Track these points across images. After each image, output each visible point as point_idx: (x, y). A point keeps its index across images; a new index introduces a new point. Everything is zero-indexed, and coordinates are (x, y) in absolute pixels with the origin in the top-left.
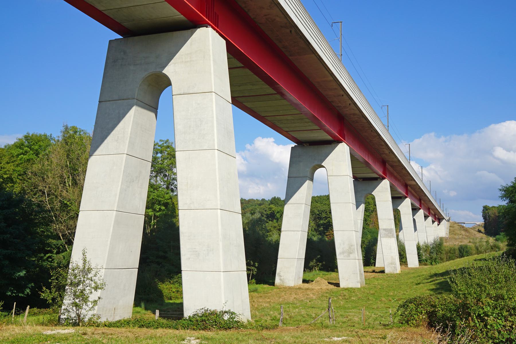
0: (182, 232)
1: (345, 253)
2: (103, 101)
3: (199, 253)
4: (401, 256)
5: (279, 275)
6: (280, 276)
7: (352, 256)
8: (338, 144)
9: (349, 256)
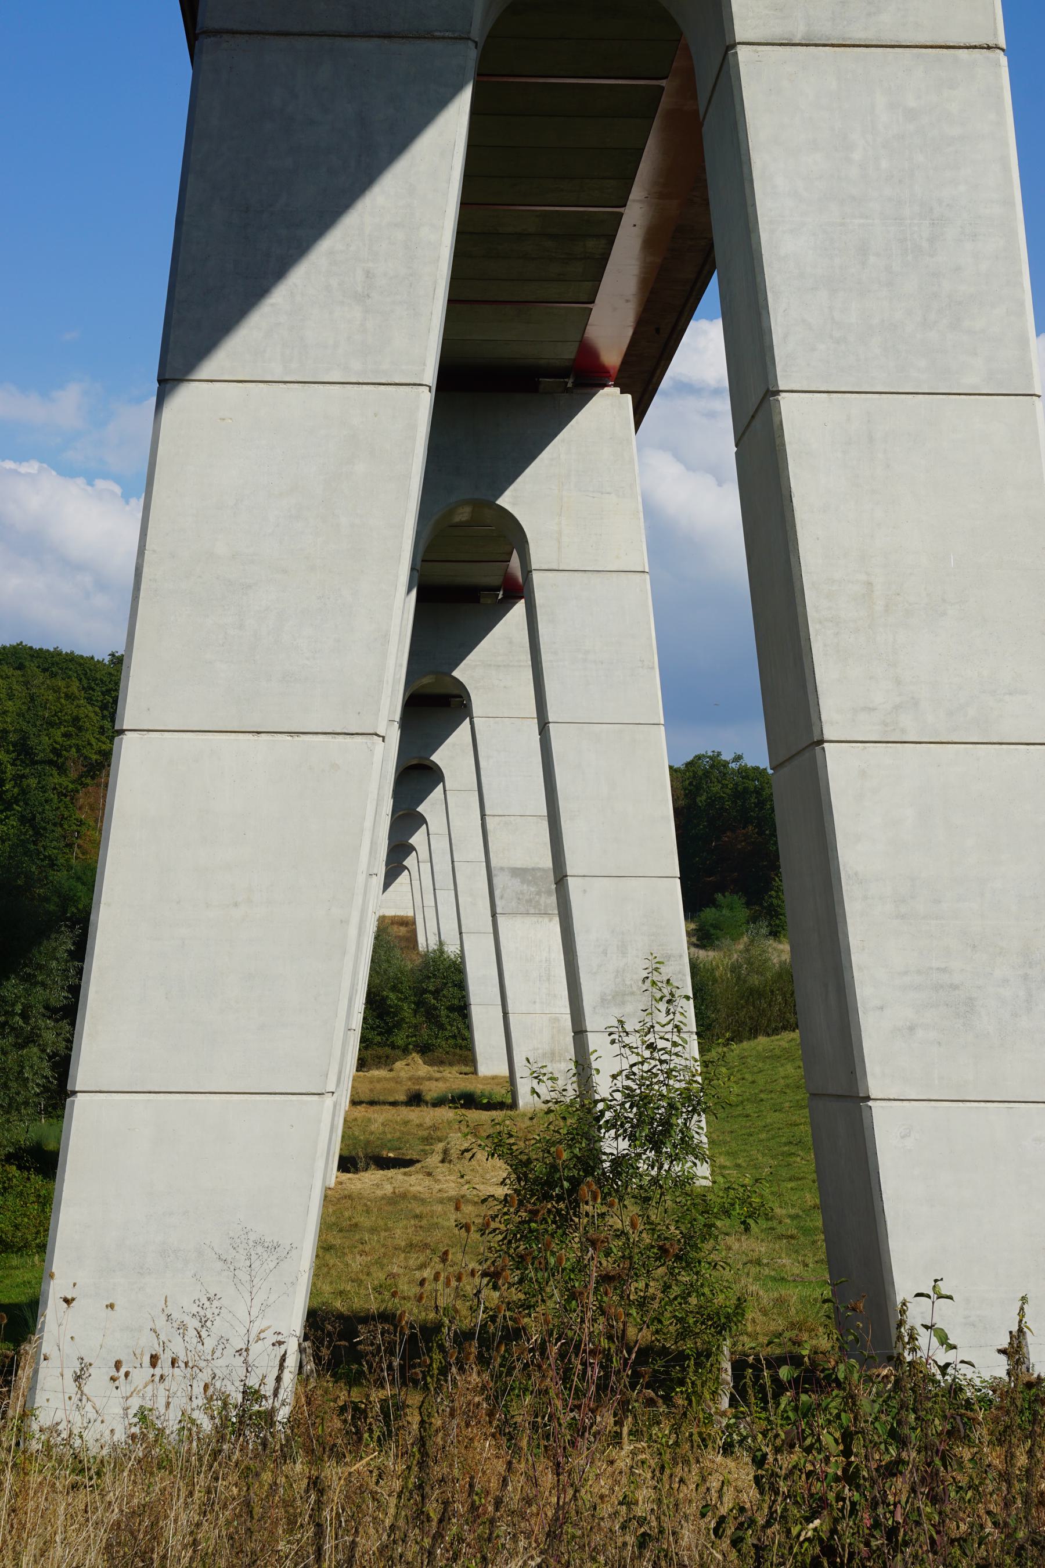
0: (856, 874)
1: (628, 998)
2: (233, 32)
3: (971, 999)
4: (388, 1013)
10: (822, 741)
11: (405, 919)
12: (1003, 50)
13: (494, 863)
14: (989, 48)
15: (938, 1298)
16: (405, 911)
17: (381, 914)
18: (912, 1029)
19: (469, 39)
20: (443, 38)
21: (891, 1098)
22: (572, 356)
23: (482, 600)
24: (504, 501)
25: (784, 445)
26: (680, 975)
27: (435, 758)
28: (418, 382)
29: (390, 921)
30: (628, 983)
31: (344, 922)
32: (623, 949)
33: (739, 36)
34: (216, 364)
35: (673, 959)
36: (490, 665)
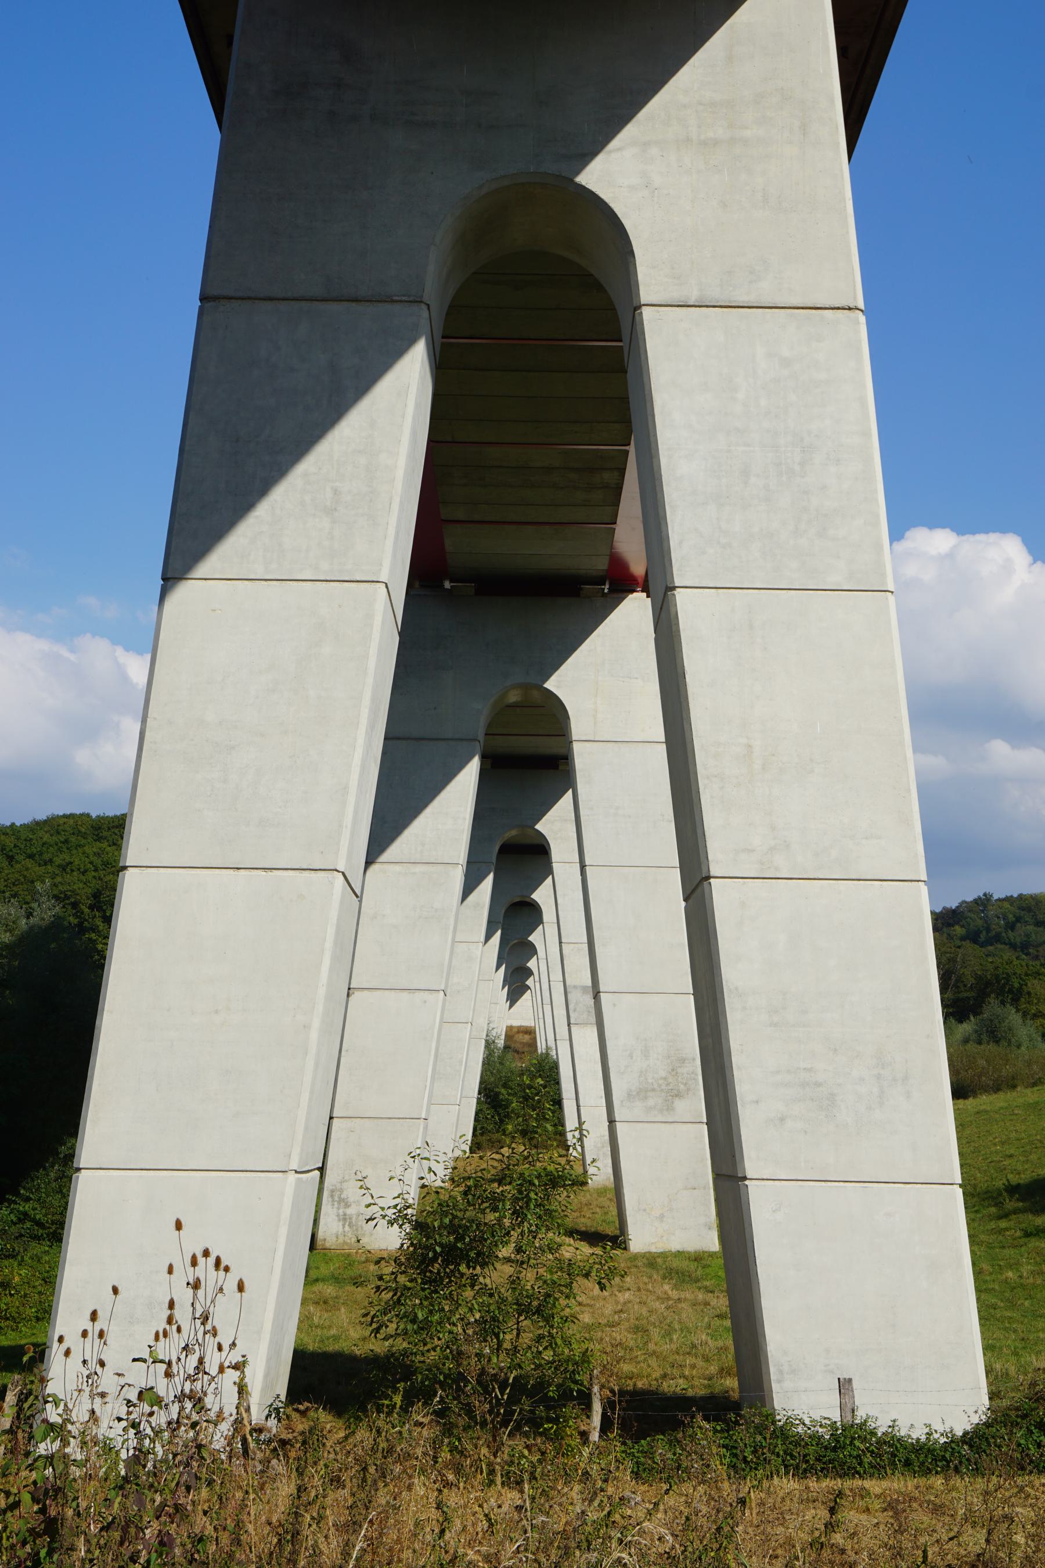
0: (737, 989)
1: (650, 1094)
2: (230, 298)
4: (501, 1106)
5: (336, 1198)
6: (341, 1200)
7: (680, 1105)
8: (620, 595)
9: (670, 1108)
10: (708, 877)
12: (862, 311)
14: (850, 309)
15: (154, 1362)
16: (528, 1022)
19: (421, 302)
20: (401, 301)
22: (606, 567)
23: (561, 767)
24: (550, 685)
25: (679, 631)
26: (693, 1075)
31: (307, 1027)
32: (646, 1053)
33: (644, 299)
34: (212, 564)
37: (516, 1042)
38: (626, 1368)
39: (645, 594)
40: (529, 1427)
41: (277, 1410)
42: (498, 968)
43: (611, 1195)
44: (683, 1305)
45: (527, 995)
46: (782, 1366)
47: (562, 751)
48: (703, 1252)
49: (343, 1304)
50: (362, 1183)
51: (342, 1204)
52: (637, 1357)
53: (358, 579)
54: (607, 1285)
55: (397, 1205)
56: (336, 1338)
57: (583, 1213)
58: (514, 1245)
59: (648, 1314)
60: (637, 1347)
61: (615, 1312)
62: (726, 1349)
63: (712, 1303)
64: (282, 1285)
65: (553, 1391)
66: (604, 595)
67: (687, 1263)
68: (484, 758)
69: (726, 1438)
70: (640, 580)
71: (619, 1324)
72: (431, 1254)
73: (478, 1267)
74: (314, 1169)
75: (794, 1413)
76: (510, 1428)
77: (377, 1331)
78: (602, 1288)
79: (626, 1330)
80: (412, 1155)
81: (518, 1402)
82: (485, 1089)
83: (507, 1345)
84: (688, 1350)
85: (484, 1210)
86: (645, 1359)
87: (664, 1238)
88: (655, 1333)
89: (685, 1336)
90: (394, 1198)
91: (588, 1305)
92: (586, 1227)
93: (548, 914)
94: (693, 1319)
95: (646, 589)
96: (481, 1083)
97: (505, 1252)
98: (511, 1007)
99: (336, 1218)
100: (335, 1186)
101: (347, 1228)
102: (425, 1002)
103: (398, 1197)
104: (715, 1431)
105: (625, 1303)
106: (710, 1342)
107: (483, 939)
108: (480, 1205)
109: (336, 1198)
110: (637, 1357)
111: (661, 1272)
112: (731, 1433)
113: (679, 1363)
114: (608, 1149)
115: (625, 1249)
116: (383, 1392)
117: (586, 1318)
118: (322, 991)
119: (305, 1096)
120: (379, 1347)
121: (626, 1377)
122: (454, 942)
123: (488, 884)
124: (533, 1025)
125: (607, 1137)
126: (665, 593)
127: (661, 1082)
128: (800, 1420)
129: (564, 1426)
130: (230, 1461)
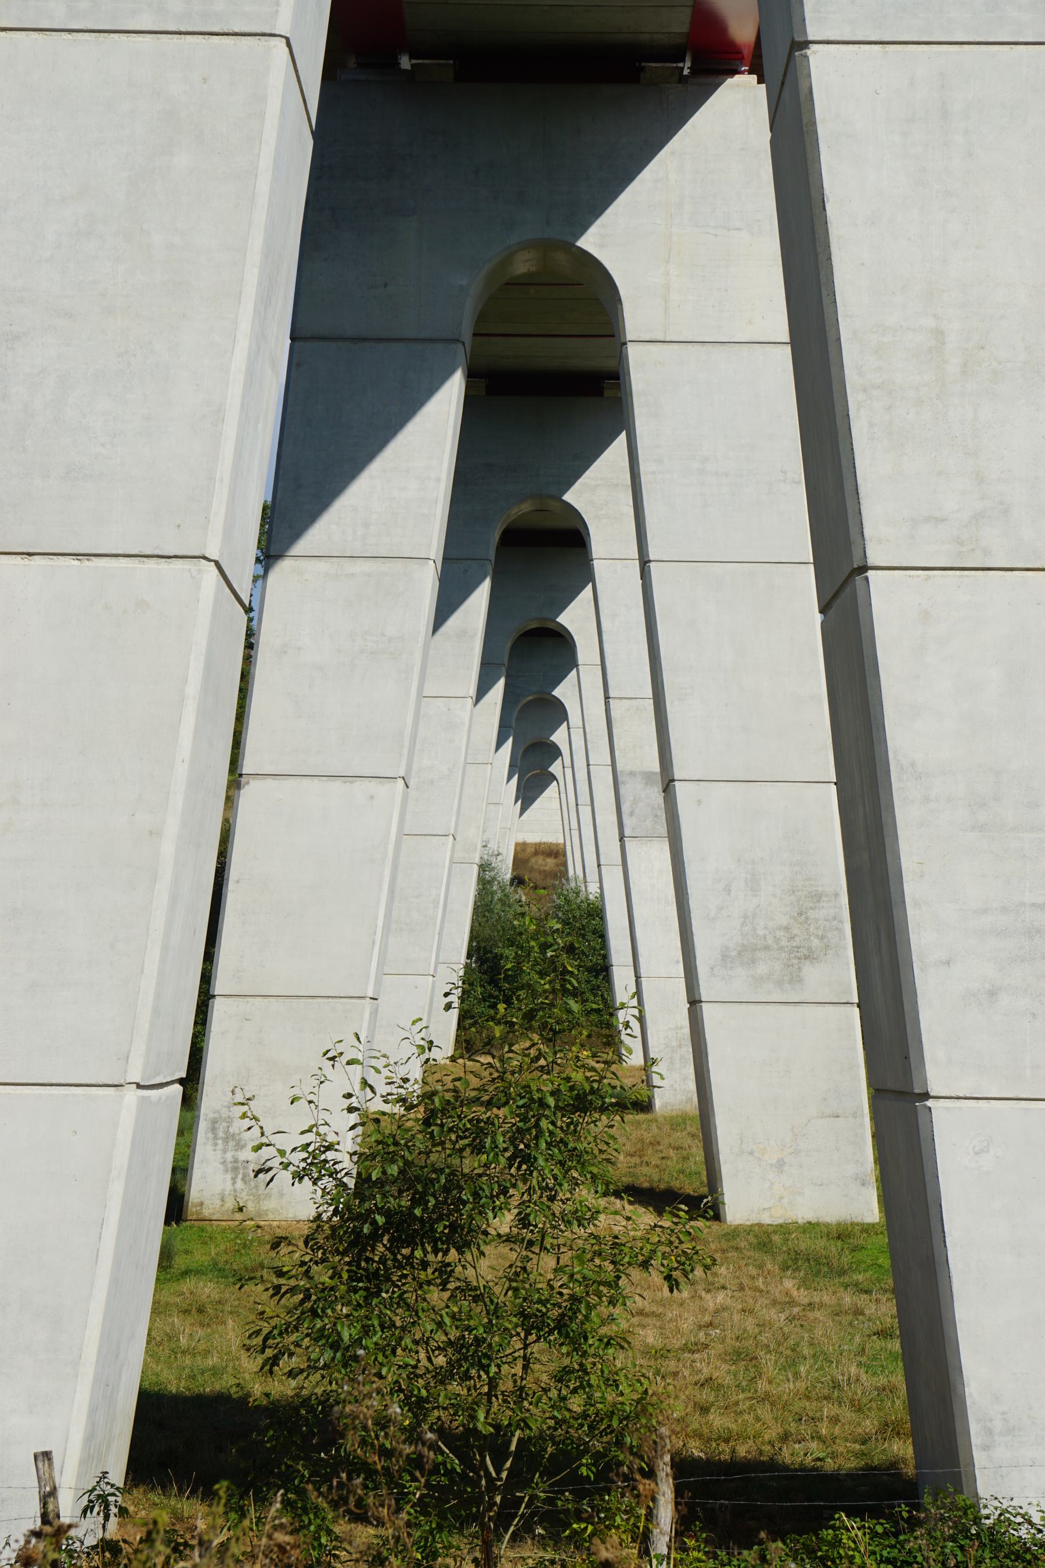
0: (913, 765)
5: (221, 1134)
7: (812, 973)
9: (796, 980)
10: (864, 569)
11: (553, 847)
13: (620, 767)
16: (552, 836)
17: (521, 841)
18: (992, 993)
21: (961, 1095)
22: (685, 29)
23: (607, 393)
24: (589, 242)
26: (835, 923)
27: (562, 619)
28: (268, 31)
29: (533, 850)
30: (761, 933)
31: (155, 833)
32: (753, 885)
35: (824, 898)
36: (617, 485)
37: (532, 870)
38: (718, 1421)
39: (754, 78)
40: (544, 1529)
41: (103, 1499)
42: (500, 744)
43: (695, 1128)
44: (818, 1314)
45: (552, 790)
46: (991, 1420)
47: (609, 364)
48: (852, 1224)
49: (231, 1313)
50: (245, 1108)
51: (232, 1143)
52: (737, 1403)
53: (237, 30)
54: (682, 1280)
55: (308, 1145)
56: (216, 1372)
57: (646, 1159)
58: (516, 1211)
59: (757, 1331)
60: (737, 1386)
61: (700, 1327)
62: (893, 1389)
63: (867, 1312)
64: (115, 1281)
65: (587, 1465)
66: (682, 79)
67: (823, 1242)
68: (472, 376)
69: (893, 1547)
70: (747, 52)
71: (707, 1346)
72: (366, 1229)
73: (453, 1251)
74: (172, 1082)
75: (1013, 1503)
76: (512, 1529)
77: (274, 1361)
78: (673, 1284)
79: (719, 1357)
80: (330, 1055)
81: (526, 1484)
82: (478, 949)
83: (506, 1385)
84: (826, 1391)
85: (462, 1150)
86: (751, 1407)
87: (785, 1201)
88: (769, 1363)
89: (821, 1368)
90: (302, 1133)
91: (653, 1314)
92: (651, 1181)
93: (586, 651)
94: (835, 1338)
95: (757, 69)
96: (472, 938)
97: (504, 1223)
98: (523, 810)
99: (221, 1167)
100: (218, 1112)
101: (239, 1184)
102: (372, 797)
103: (309, 1131)
104: (874, 1535)
105: (717, 1311)
106: (864, 1377)
107: (472, 691)
108: (454, 1143)
109: (221, 1134)
110: (737, 1403)
111: (780, 1259)
112: (902, 1538)
113: (811, 1414)
114: (688, 1051)
115: (717, 1217)
116: (288, 1467)
117: (650, 1336)
118: (181, 771)
119: (153, 956)
120: (282, 1388)
121: (719, 1438)
122: (421, 696)
123: (480, 598)
124: (561, 841)
125: (687, 1030)
126: (790, 56)
127: (780, 934)
128: (1023, 1517)
129: (607, 1527)
130: (688, 1279)
